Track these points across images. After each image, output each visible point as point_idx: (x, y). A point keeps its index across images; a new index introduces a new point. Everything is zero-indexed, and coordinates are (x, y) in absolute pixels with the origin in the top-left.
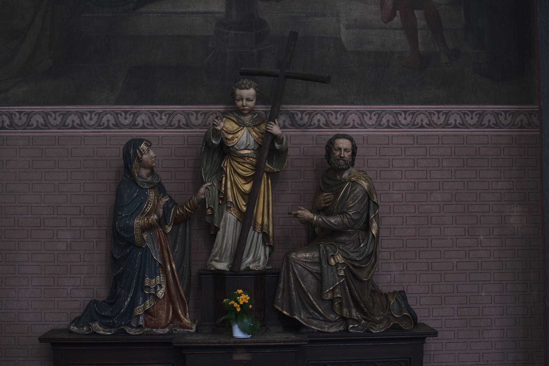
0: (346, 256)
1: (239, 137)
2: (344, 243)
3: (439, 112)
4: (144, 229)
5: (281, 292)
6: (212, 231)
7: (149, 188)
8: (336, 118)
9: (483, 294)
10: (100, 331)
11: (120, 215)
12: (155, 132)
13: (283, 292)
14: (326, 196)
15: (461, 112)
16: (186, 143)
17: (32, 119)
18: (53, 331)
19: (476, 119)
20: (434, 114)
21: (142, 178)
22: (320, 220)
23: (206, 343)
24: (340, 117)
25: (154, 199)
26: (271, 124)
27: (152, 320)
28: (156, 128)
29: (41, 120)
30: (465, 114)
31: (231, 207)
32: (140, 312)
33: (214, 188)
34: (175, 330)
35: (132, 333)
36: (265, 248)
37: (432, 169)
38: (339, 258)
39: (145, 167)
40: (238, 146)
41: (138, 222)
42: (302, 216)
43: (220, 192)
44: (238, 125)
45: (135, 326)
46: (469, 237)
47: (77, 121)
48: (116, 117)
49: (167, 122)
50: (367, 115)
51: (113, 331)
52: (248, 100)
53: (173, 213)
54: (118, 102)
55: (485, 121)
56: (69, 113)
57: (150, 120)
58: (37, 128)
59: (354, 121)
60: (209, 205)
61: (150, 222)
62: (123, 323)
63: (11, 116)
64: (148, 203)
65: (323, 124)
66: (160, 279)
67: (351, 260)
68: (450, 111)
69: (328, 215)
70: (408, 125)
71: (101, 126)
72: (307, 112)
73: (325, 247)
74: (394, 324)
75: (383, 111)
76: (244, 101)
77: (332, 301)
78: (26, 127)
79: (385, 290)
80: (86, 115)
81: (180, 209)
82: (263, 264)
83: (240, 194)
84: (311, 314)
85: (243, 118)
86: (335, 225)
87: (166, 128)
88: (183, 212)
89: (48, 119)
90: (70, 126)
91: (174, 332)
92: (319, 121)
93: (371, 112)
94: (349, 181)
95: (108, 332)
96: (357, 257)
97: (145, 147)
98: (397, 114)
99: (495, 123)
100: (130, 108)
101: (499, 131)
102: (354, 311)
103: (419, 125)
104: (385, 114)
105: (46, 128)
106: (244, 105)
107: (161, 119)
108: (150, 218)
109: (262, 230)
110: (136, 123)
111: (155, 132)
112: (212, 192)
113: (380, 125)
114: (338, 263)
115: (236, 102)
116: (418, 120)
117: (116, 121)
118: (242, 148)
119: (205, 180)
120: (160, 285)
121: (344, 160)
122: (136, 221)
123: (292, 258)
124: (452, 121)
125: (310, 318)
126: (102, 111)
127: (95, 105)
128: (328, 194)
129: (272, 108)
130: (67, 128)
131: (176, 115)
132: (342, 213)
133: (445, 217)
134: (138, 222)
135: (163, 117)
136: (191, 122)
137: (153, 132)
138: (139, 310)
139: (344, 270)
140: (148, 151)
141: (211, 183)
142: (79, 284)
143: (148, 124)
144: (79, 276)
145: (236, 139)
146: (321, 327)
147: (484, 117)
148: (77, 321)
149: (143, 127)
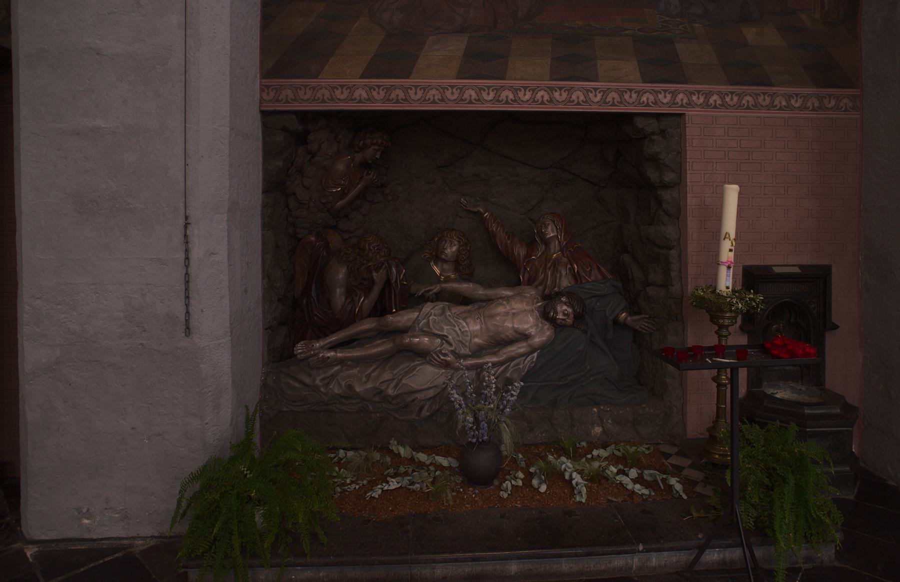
15: (477, 88)
20: (448, 89)
50: (374, 90)
56: (394, 88)
80: (728, 95)
116: (319, 95)
147: (501, 93)
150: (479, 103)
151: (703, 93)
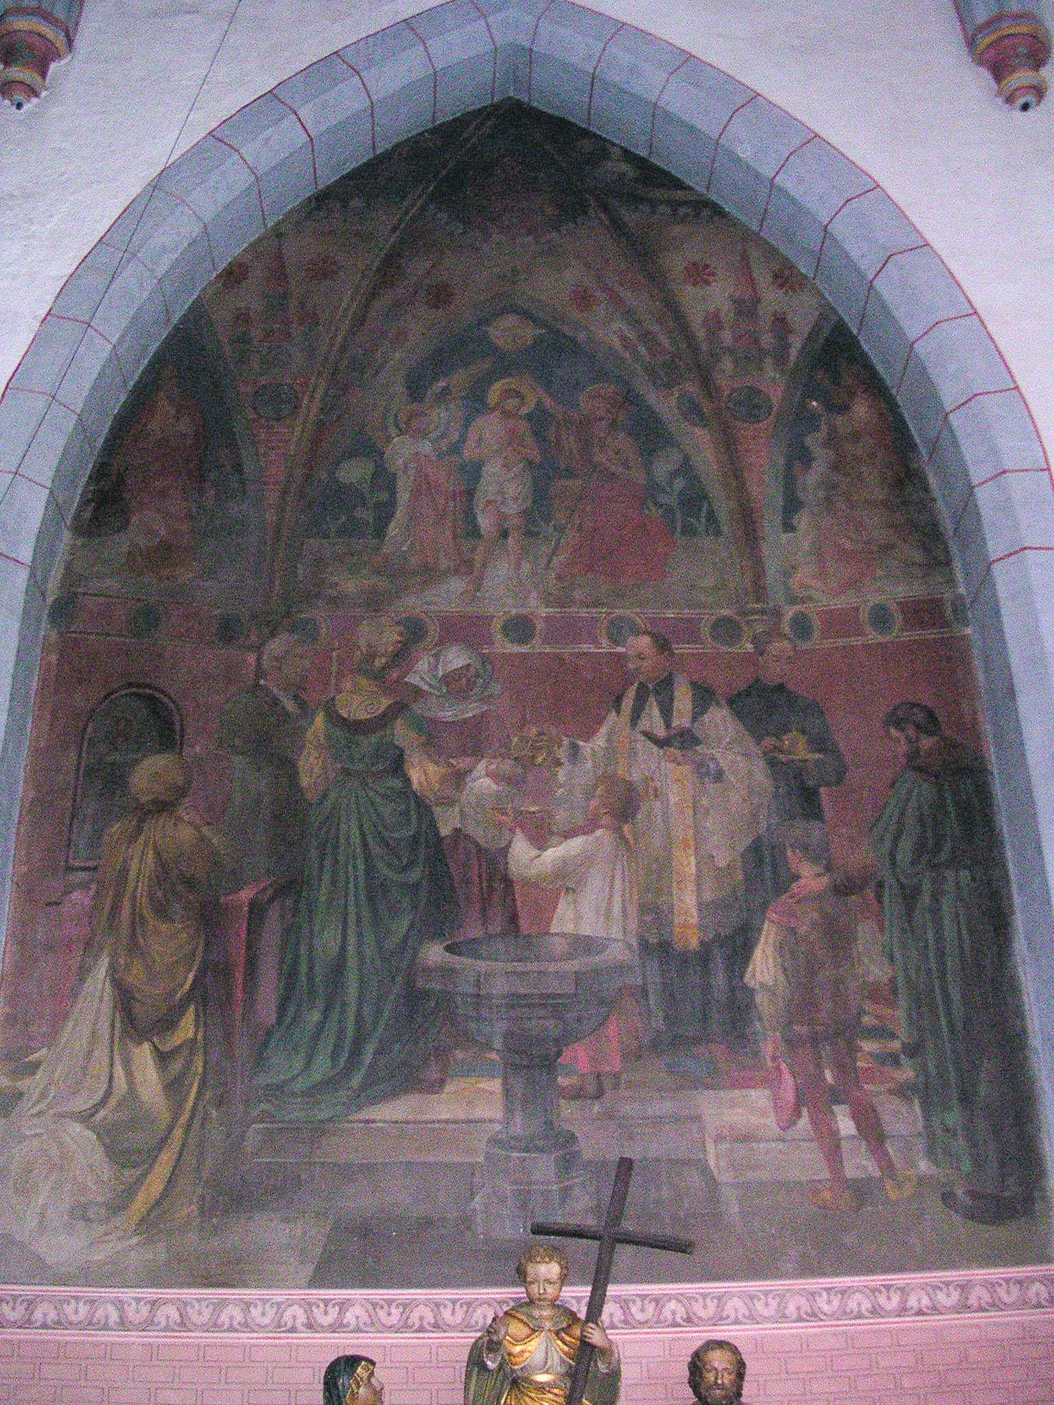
8: (705, 1307)
47: (239, 1317)
49: (399, 1320)
54: (315, 1282)
55: (973, 1301)
93: (766, 1293)
116: (852, 1305)
135: (393, 1310)
149: (358, 1330)
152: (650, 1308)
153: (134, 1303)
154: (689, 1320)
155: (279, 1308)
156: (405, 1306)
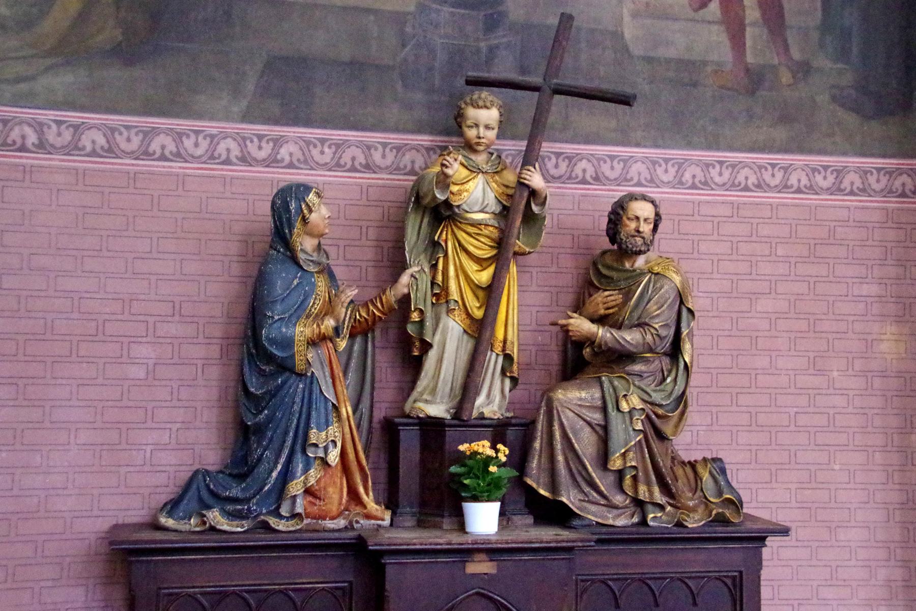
0: (646, 397)
1: (471, 191)
2: (640, 375)
3: (773, 166)
4: (312, 343)
5: (537, 457)
6: (415, 350)
7: (316, 272)
8: (612, 168)
9: (837, 467)
10: (223, 525)
11: (269, 317)
12: (312, 175)
13: (540, 456)
14: (607, 296)
16: (364, 196)
17: (83, 136)
18: (116, 527)
19: (831, 179)
20: (766, 169)
21: (306, 253)
22: (608, 335)
23: (426, 545)
24: (619, 167)
25: (325, 292)
26: (529, 170)
27: (315, 505)
28: (312, 169)
29: (101, 141)
30: (814, 170)
31: (455, 309)
32: (298, 490)
33: (424, 276)
34: (357, 522)
35: (281, 528)
36: (503, 382)
37: (759, 258)
38: (634, 401)
39: (311, 234)
40: (467, 205)
41: (302, 331)
42: (578, 329)
43: (433, 283)
44: (468, 169)
45: (288, 515)
46: (816, 372)
47: (171, 147)
48: (243, 145)
51: (246, 525)
52: (487, 127)
53: (350, 318)
54: (246, 117)
55: (846, 184)
57: (304, 154)
58: (94, 153)
59: (639, 174)
60: (416, 304)
61: (323, 331)
62: (264, 511)
63: (39, 128)
64: (316, 298)
65: (591, 176)
66: (334, 431)
67: (652, 404)
68: (791, 165)
69: (619, 326)
70: (724, 184)
71: (215, 158)
72: (268, 137)
73: (611, 383)
74: (718, 514)
75: (686, 160)
76: (482, 129)
77: (620, 474)
78: (72, 150)
79: (686, 456)
81: (361, 310)
82: (500, 408)
83: (471, 288)
84: (586, 494)
85: (473, 157)
86: (631, 344)
87: (330, 170)
88: (368, 315)
89: (115, 139)
90: (157, 156)
91: (356, 526)
92: (584, 171)
93: (666, 161)
94: (650, 272)
95: (238, 527)
96: (662, 399)
97: (315, 198)
98: (708, 165)
99: (861, 187)
100: (268, 130)
101: (867, 201)
102: (656, 490)
103: (742, 186)
104: (690, 166)
105: (111, 155)
106: (482, 135)
107: (322, 153)
108: (322, 324)
109: (504, 350)
110: (279, 157)
111: (312, 175)
112: (422, 283)
113: (681, 183)
114: (634, 408)
115: (466, 129)
116: (741, 178)
117: (242, 151)
118: (476, 209)
119: (410, 261)
120: (334, 442)
121: (643, 238)
122: (299, 329)
123: (558, 399)
124: (793, 181)
125: (584, 501)
126: (217, 133)
127: (204, 120)
128: (611, 293)
129: (527, 146)
130: (152, 158)
131: (349, 147)
132: (641, 325)
133: (779, 339)
134: (302, 331)
135: (326, 150)
136: (374, 161)
137: (308, 175)
138: (296, 487)
139: (642, 421)
140: (319, 205)
141: (420, 268)
142: (168, 442)
143: (298, 160)
144: (168, 426)
145: (465, 194)
146: (602, 517)
148: (172, 506)
149: (291, 165)
150: (705, 187)
151: (833, 170)
152: (563, 166)
153: (54, 126)
154: (597, 179)
155: (212, 142)
156: (338, 146)
